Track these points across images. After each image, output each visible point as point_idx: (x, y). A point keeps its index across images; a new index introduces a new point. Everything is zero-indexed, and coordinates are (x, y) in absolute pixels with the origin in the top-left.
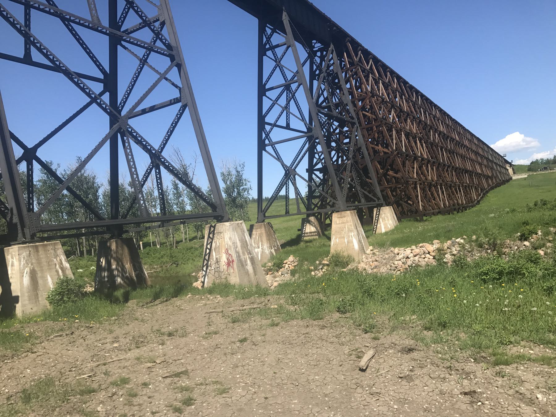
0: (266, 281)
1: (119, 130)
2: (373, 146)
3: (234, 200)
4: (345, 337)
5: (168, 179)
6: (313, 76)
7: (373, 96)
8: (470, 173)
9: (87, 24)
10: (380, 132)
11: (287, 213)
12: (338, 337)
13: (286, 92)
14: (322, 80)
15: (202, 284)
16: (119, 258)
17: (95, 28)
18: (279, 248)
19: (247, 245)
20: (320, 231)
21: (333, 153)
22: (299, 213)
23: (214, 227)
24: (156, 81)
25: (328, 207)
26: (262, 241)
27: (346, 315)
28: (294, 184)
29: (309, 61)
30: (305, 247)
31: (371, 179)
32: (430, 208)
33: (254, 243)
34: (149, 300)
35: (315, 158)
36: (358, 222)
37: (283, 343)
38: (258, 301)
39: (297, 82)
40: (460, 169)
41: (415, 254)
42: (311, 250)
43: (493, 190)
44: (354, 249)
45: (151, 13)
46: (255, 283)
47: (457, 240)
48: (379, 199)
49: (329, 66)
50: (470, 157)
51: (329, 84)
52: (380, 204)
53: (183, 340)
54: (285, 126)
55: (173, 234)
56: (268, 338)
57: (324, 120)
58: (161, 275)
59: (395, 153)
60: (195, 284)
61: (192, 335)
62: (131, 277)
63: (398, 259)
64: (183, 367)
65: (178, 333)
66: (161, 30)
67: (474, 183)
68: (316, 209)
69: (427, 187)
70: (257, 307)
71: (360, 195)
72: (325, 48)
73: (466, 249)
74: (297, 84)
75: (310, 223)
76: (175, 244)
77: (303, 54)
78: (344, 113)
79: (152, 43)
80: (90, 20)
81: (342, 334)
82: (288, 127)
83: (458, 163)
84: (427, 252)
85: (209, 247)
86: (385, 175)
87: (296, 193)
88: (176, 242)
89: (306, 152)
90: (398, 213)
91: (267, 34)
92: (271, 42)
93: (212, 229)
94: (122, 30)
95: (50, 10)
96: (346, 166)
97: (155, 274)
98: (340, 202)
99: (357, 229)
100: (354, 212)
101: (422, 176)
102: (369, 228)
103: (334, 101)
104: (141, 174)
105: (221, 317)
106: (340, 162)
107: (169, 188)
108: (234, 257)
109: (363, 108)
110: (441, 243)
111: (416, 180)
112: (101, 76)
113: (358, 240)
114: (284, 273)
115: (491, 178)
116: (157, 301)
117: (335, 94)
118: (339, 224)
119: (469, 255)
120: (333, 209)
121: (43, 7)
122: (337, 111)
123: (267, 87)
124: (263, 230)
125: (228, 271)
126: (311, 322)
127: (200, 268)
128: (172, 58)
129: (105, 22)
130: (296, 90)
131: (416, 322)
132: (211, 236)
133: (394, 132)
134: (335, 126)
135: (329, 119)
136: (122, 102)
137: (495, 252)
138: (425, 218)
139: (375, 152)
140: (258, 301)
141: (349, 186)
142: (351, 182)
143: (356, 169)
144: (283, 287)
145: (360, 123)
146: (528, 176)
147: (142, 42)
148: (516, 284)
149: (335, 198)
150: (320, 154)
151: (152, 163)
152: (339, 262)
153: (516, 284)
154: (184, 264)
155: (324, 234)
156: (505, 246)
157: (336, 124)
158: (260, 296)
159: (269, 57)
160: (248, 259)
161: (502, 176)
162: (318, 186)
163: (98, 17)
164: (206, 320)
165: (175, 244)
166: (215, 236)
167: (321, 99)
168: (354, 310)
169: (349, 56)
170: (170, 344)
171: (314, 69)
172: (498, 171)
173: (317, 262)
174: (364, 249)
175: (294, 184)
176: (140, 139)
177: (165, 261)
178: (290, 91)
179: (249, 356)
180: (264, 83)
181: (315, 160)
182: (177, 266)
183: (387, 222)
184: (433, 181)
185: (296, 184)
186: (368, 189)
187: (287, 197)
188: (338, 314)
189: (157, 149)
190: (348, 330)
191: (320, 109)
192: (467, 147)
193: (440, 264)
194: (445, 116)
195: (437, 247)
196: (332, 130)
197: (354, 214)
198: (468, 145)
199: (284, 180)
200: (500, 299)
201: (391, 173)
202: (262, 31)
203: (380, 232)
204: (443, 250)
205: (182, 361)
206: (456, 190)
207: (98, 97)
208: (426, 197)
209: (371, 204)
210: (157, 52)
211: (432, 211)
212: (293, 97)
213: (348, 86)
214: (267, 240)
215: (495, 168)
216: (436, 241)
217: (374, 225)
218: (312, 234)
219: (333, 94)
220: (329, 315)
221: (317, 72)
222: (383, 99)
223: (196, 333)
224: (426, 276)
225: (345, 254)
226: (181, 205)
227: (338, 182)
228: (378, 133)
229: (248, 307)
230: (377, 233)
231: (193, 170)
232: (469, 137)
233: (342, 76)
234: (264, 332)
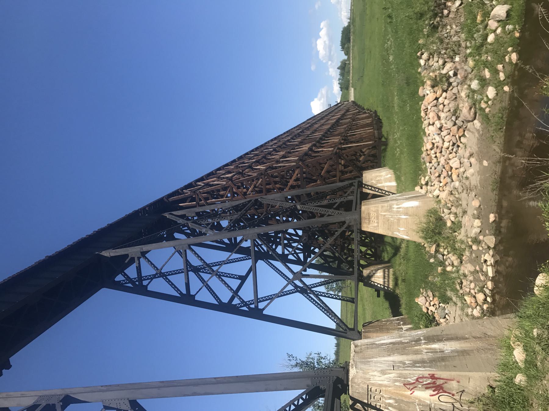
18: (402, 318)
19: (401, 343)
20: (383, 265)
23: (355, 401)
36: (379, 199)
41: (436, 118)
44: (417, 207)
47: (422, 62)
48: (351, 185)
52: (358, 184)
82: (243, 279)
84: (435, 101)
98: (348, 218)
108: (425, 372)
113: (405, 201)
114: (443, 315)
118: (378, 223)
123: (184, 292)
125: (454, 392)
138: (383, 140)
146: (352, 87)
160: (429, 346)
166: (373, 404)
169: (184, 201)
178: (202, 268)
180: (179, 295)
183: (382, 178)
202: (119, 286)
203: (395, 188)
214: (388, 333)
216: (421, 92)
218: (386, 275)
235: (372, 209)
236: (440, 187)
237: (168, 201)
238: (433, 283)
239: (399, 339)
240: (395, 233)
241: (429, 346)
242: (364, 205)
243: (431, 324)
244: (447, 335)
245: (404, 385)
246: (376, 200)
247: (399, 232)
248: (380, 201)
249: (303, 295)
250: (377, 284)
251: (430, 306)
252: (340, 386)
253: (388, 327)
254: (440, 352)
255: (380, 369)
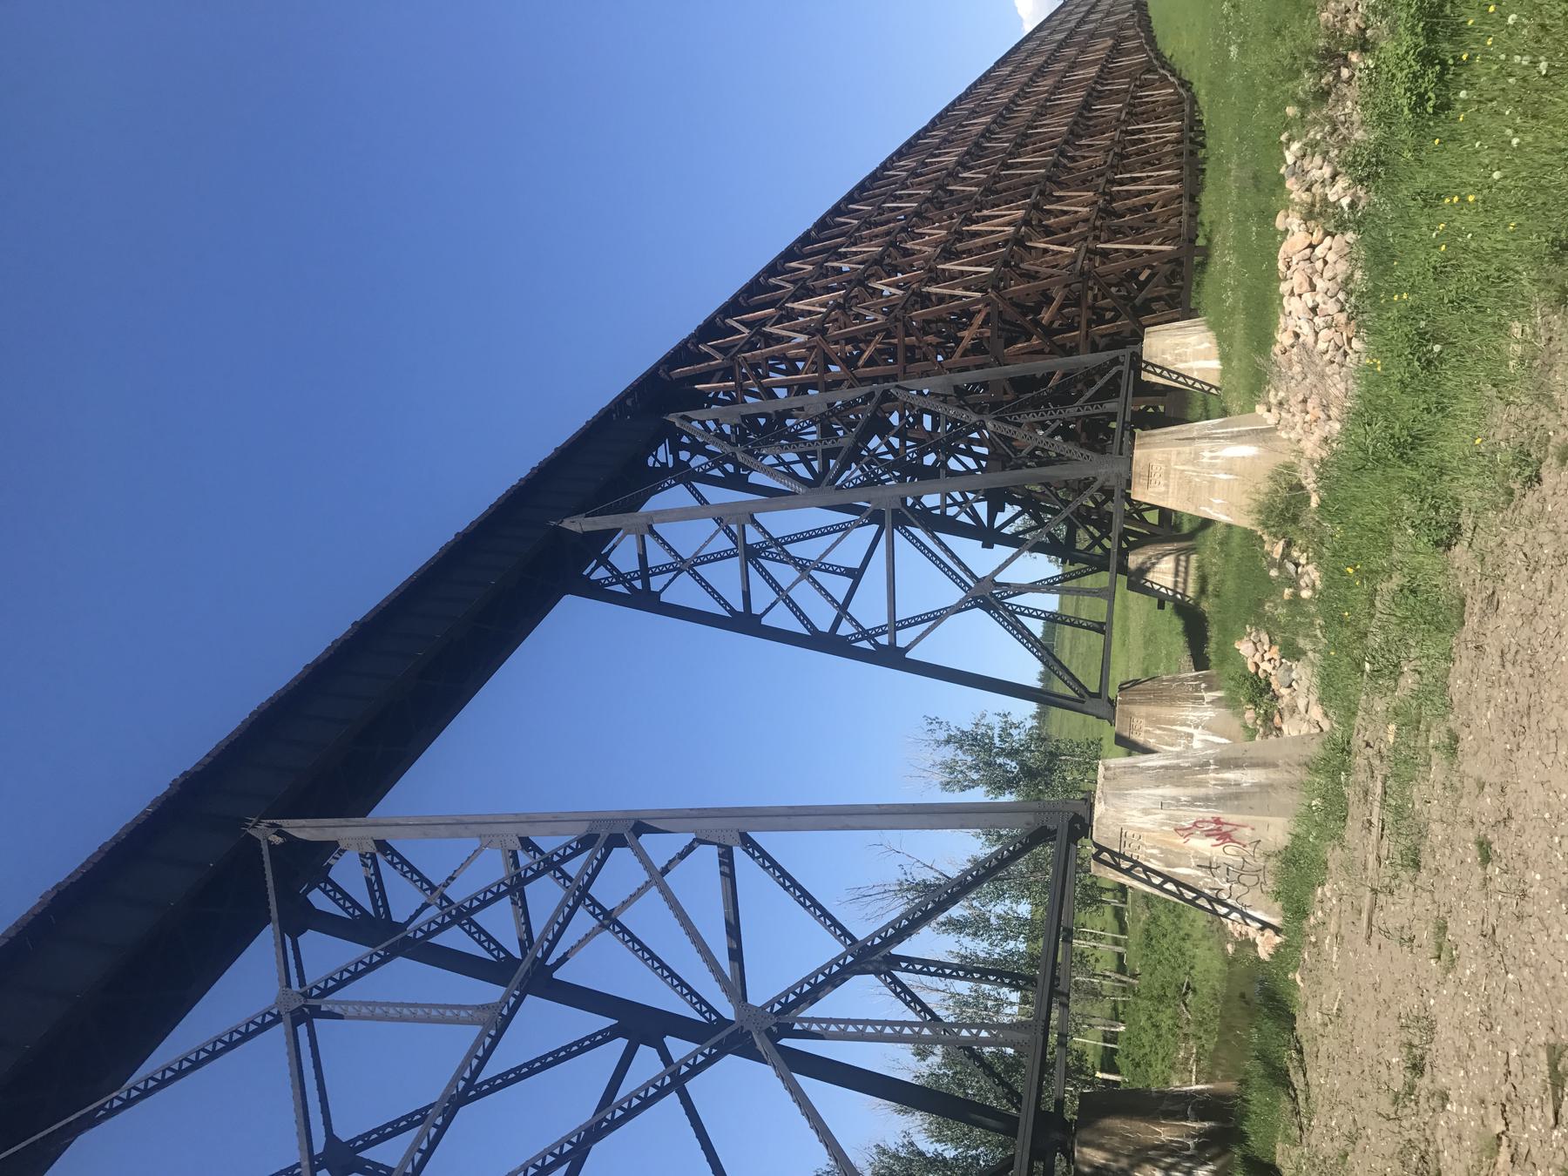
0: (1302, 740)
1: (773, 1038)
2: (959, 351)
3: (1029, 773)
4: (1541, 546)
5: (929, 943)
6: (737, 481)
7: (824, 331)
8: (1094, 95)
9: (488, 1041)
10: (923, 328)
11: (1101, 628)
12: (1533, 567)
13: (762, 561)
14: (752, 459)
15: (1269, 933)
16: (1137, 1151)
17: (499, 1022)
18: (1205, 676)
19: (1178, 767)
20: (1176, 545)
21: (953, 464)
22: (1108, 594)
23: (1101, 849)
24: (666, 899)
25: (1109, 507)
26: (1173, 722)
27: (1464, 527)
28: (1020, 590)
29: (696, 485)
30: (1217, 601)
31: (1054, 373)
32: (1173, 221)
33: (1172, 745)
34: (1286, 1104)
35: (956, 516)
36: (1172, 432)
37: (1519, 732)
38: (1362, 777)
39: (743, 526)
40: (1076, 123)
41: (1306, 286)
42: (1230, 584)
43: (1158, 39)
44: (1253, 458)
45: (492, 869)
46: (1299, 774)
47: (1290, 159)
48: (1115, 362)
49: (721, 436)
50: (1046, 92)
51: (767, 443)
53: (1443, 1032)
54: (849, 581)
55: (1094, 975)
56: (1493, 777)
57: (858, 473)
58: (1210, 1047)
59: (992, 294)
60: (1264, 952)
61: (1432, 1002)
62: (1200, 1136)
63: (1310, 339)
64: (1536, 1056)
65: (1416, 1042)
66: (541, 853)
67: (1126, 91)
68: (1106, 542)
69: (1108, 222)
70: (1384, 783)
71: (1093, 411)
72: (674, 438)
73: (1324, 138)
74: (749, 528)
75: (1148, 570)
76: (1124, 979)
77: (676, 496)
78: (852, 417)
79: (568, 884)
80: (480, 1028)
81: (1527, 549)
82: (856, 575)
83: (1056, 126)
84: (1308, 251)
85: (1157, 880)
86: (1049, 332)
87: (1048, 591)
88: (1118, 972)
89: (935, 538)
90: (1169, 314)
91: (607, 579)
92: (629, 573)
93: (1105, 856)
94: (518, 955)
95: (435, 1126)
96: (1000, 436)
97: (1204, 1063)
98: (1103, 471)
99: (1193, 439)
100: (1141, 437)
101: (1073, 232)
102: (1199, 403)
103: (814, 437)
104: (900, 1011)
105: (1390, 900)
106: (984, 451)
107: (956, 948)
108: (1207, 814)
109: (849, 362)
110: (1287, 208)
111: (1083, 250)
112: (620, 1044)
115: (1120, 40)
116: (1294, 1080)
117: (796, 430)
118: (1167, 486)
119: (1345, 132)
120: (1117, 494)
121: (425, 1141)
122: (841, 433)
123: (739, 608)
124: (1140, 710)
125: (1246, 842)
126: (1467, 633)
127: (1216, 925)
128: (616, 841)
129: (491, 993)
130: (765, 532)
131: (1533, 326)
132: (1125, 865)
133: (933, 289)
134: (880, 446)
135: (858, 458)
136: (698, 1006)
137: (1349, 56)
138: (1201, 242)
139: (978, 348)
140: (1362, 777)
141: (1058, 438)
142: (1049, 431)
143: (1014, 409)
144: (1332, 691)
145: (886, 379)
147: (559, 910)
148: (1470, 23)
149: (1086, 484)
150: (949, 501)
151: (878, 974)
152: (1287, 509)
153: (1470, 23)
154: (1192, 968)
155: (1191, 536)
156: (1338, 25)
157: (875, 442)
158: (1345, 767)
159: (666, 586)
160: (1220, 776)
161: (1120, 9)
162: (1041, 524)
163: (478, 1008)
164: (1394, 945)
165: (1124, 979)
166: (1128, 854)
167: (801, 470)
168: (1457, 502)
169: (706, 377)
170: (1446, 1076)
171: (720, 474)
172: (1102, 19)
173: (1274, 573)
174: (1262, 430)
175: (1020, 590)
176: (807, 988)
177: (1170, 1022)
178: (764, 550)
179: (1542, 845)
181: (964, 518)
182: (1194, 991)
184: (1096, 202)
185: (1021, 586)
186: (1080, 386)
187: (1052, 619)
188: (1457, 550)
189: (843, 949)
190: (1516, 530)
191: (826, 481)
192: (1017, 95)
193: (1359, 223)
194: (917, 145)
195: (1298, 221)
196: (890, 457)
197: (1147, 439)
198: (1011, 94)
199: (1000, 615)
200: (1510, 75)
201: (1046, 316)
202: (597, 591)
203: (1217, 375)
204: (1313, 205)
205: (1514, 1053)
206: (1134, 143)
207: (671, 1069)
208: (1138, 229)
209: (1126, 385)
210: (592, 878)
211: (1184, 218)
212: (781, 545)
213: (781, 393)
214: (1171, 706)
215: (1092, 26)
216: (1280, 223)
217: (1192, 386)
218: (1182, 569)
219: (794, 438)
220: (1456, 576)
221: (730, 468)
222: (838, 306)
223: (1429, 986)
224: (1389, 270)
225: (1265, 487)
226: (1009, 926)
227: (1040, 465)
228: (927, 334)
229: (1376, 810)
230: (1217, 384)
231: (919, 865)
232: (988, 87)
233: (753, 405)
234: (1470, 784)
235: (1156, 456)
236: (1305, 423)
237: (670, 376)
238: (1273, 620)
239: (1175, 761)
240: (1202, 508)
241: (1220, 776)
242: (1142, 446)
243: (1261, 696)
244: (1251, 758)
245: (1176, 830)
246: (1166, 433)
247: (1211, 508)
248: (1175, 436)
249: (989, 613)
250: (1157, 587)
251: (1263, 660)
252: (1078, 826)
253: (1172, 693)
254: (1235, 785)
255: (1140, 807)
